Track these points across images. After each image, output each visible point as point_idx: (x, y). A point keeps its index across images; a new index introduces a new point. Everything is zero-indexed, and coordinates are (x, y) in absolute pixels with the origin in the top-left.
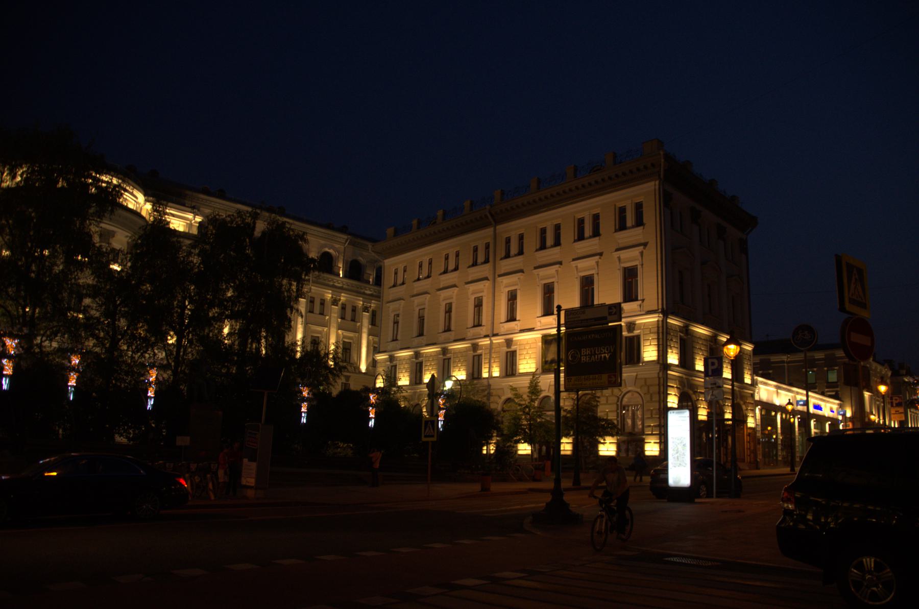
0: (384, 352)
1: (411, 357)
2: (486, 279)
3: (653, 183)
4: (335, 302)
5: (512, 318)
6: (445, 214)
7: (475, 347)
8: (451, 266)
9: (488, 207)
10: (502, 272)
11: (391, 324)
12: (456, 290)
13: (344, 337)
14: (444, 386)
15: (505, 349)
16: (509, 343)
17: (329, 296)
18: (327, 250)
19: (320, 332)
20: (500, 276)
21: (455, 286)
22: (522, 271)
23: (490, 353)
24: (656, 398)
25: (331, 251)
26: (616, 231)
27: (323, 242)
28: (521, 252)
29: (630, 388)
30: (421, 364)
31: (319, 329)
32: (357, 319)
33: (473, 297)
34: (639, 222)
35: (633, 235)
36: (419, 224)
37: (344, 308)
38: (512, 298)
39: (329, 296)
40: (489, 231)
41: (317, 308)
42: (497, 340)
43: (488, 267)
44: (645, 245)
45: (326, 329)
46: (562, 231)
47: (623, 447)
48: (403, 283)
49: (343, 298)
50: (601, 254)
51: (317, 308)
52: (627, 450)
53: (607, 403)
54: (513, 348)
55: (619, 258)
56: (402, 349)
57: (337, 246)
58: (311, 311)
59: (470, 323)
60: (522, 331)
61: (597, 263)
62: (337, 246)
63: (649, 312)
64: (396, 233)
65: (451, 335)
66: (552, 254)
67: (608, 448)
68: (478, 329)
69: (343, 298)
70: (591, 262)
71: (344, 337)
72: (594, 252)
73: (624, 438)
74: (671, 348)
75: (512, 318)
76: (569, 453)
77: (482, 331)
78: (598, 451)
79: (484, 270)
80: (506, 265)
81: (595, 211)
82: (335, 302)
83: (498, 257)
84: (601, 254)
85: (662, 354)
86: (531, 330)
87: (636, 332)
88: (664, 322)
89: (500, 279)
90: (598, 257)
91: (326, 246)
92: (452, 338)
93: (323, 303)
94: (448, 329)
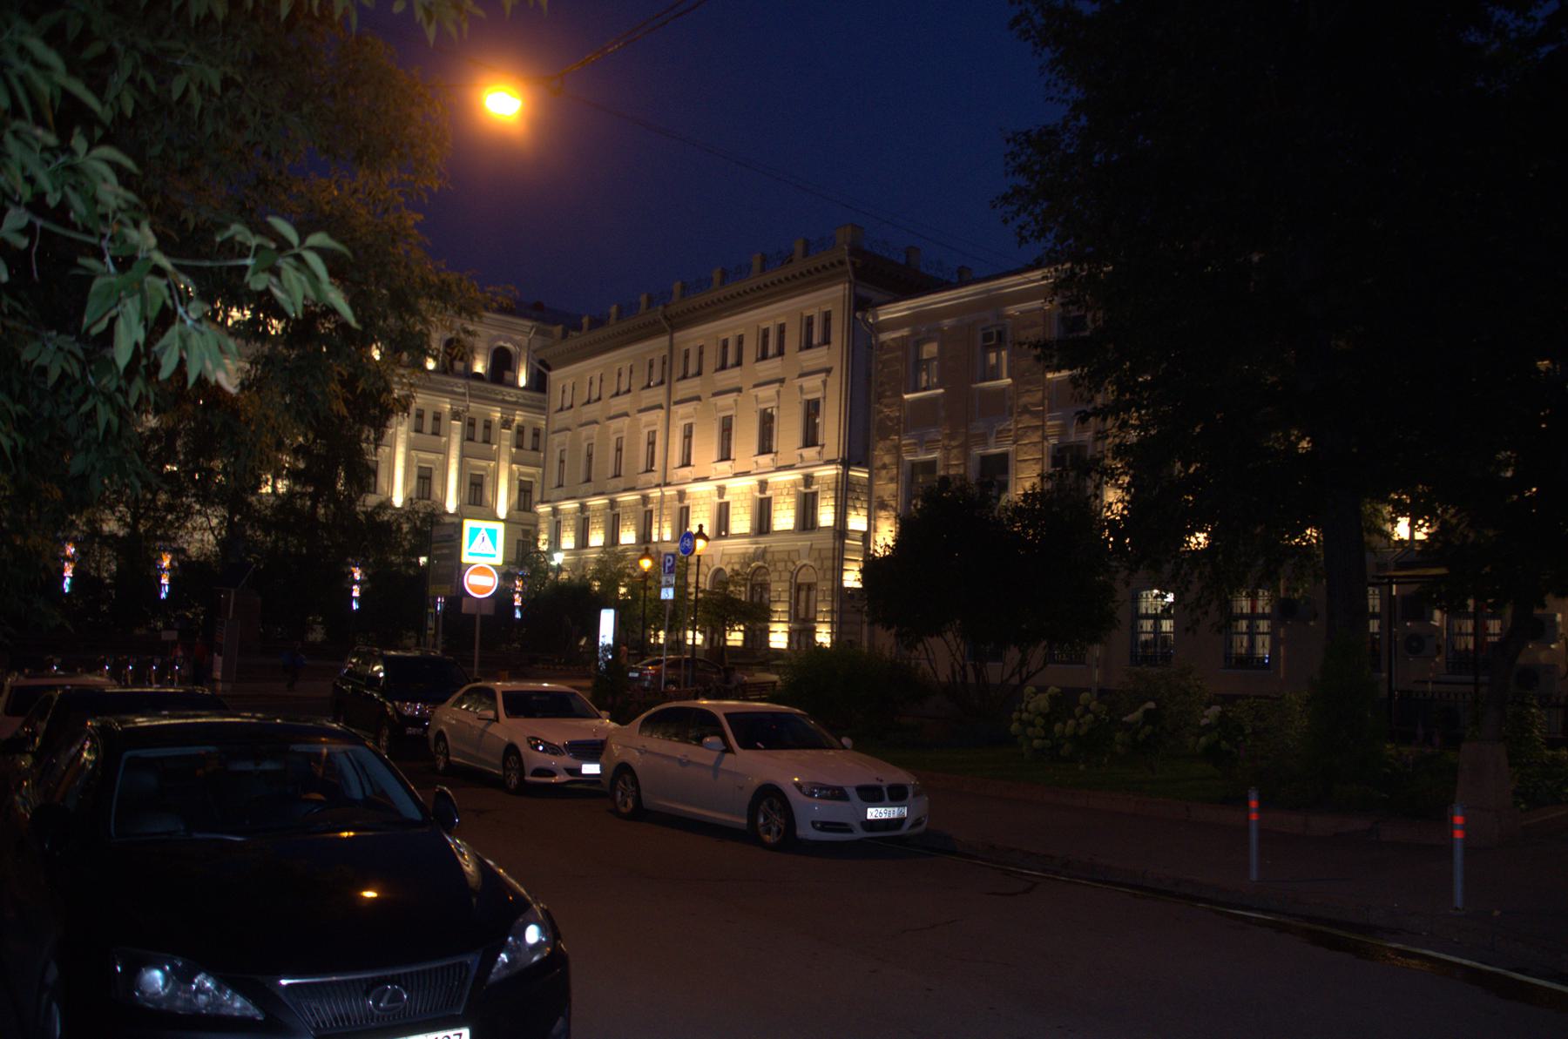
0: (601, 494)
1: (605, 507)
2: (660, 407)
3: (841, 287)
4: (506, 424)
5: (686, 463)
6: (807, 245)
7: (645, 500)
8: (692, 369)
9: (660, 308)
10: (557, 427)
11: (556, 464)
12: (627, 420)
13: (521, 474)
14: (552, 559)
15: (677, 505)
16: (682, 495)
17: (497, 415)
18: (502, 344)
19: (484, 469)
20: (677, 403)
21: (626, 414)
22: (698, 398)
23: (661, 509)
24: (829, 575)
25: (508, 345)
26: (801, 349)
27: (495, 333)
28: (739, 363)
29: (805, 562)
30: (559, 522)
31: (483, 463)
32: (541, 447)
33: (683, 423)
34: (826, 341)
35: (817, 357)
36: (724, 274)
37: (520, 431)
38: (688, 436)
39: (497, 415)
40: (663, 341)
41: (479, 435)
42: (670, 492)
43: (662, 390)
44: (828, 371)
45: (492, 464)
46: (787, 334)
47: (795, 638)
48: (629, 391)
49: (519, 417)
50: (782, 381)
51: (479, 435)
52: (798, 642)
53: (780, 580)
54: (686, 502)
55: (801, 388)
56: (595, 495)
57: (518, 338)
58: (471, 439)
59: (642, 467)
60: (696, 480)
61: (778, 393)
62: (518, 338)
63: (829, 462)
64: (725, 277)
65: (590, 487)
66: (731, 377)
67: (735, 638)
68: (686, 470)
69: (519, 417)
70: (770, 391)
71: (521, 474)
72: (774, 377)
73: (796, 626)
74: (855, 508)
75: (686, 463)
76: (739, 644)
77: (656, 477)
78: (768, 642)
79: (658, 395)
80: (683, 389)
81: (781, 320)
82: (506, 424)
83: (675, 378)
84: (782, 381)
85: (841, 516)
86: (705, 479)
87: (814, 488)
88: (845, 475)
89: (673, 408)
90: (777, 385)
91: (499, 338)
92: (622, 486)
93: (488, 425)
94: (588, 480)
